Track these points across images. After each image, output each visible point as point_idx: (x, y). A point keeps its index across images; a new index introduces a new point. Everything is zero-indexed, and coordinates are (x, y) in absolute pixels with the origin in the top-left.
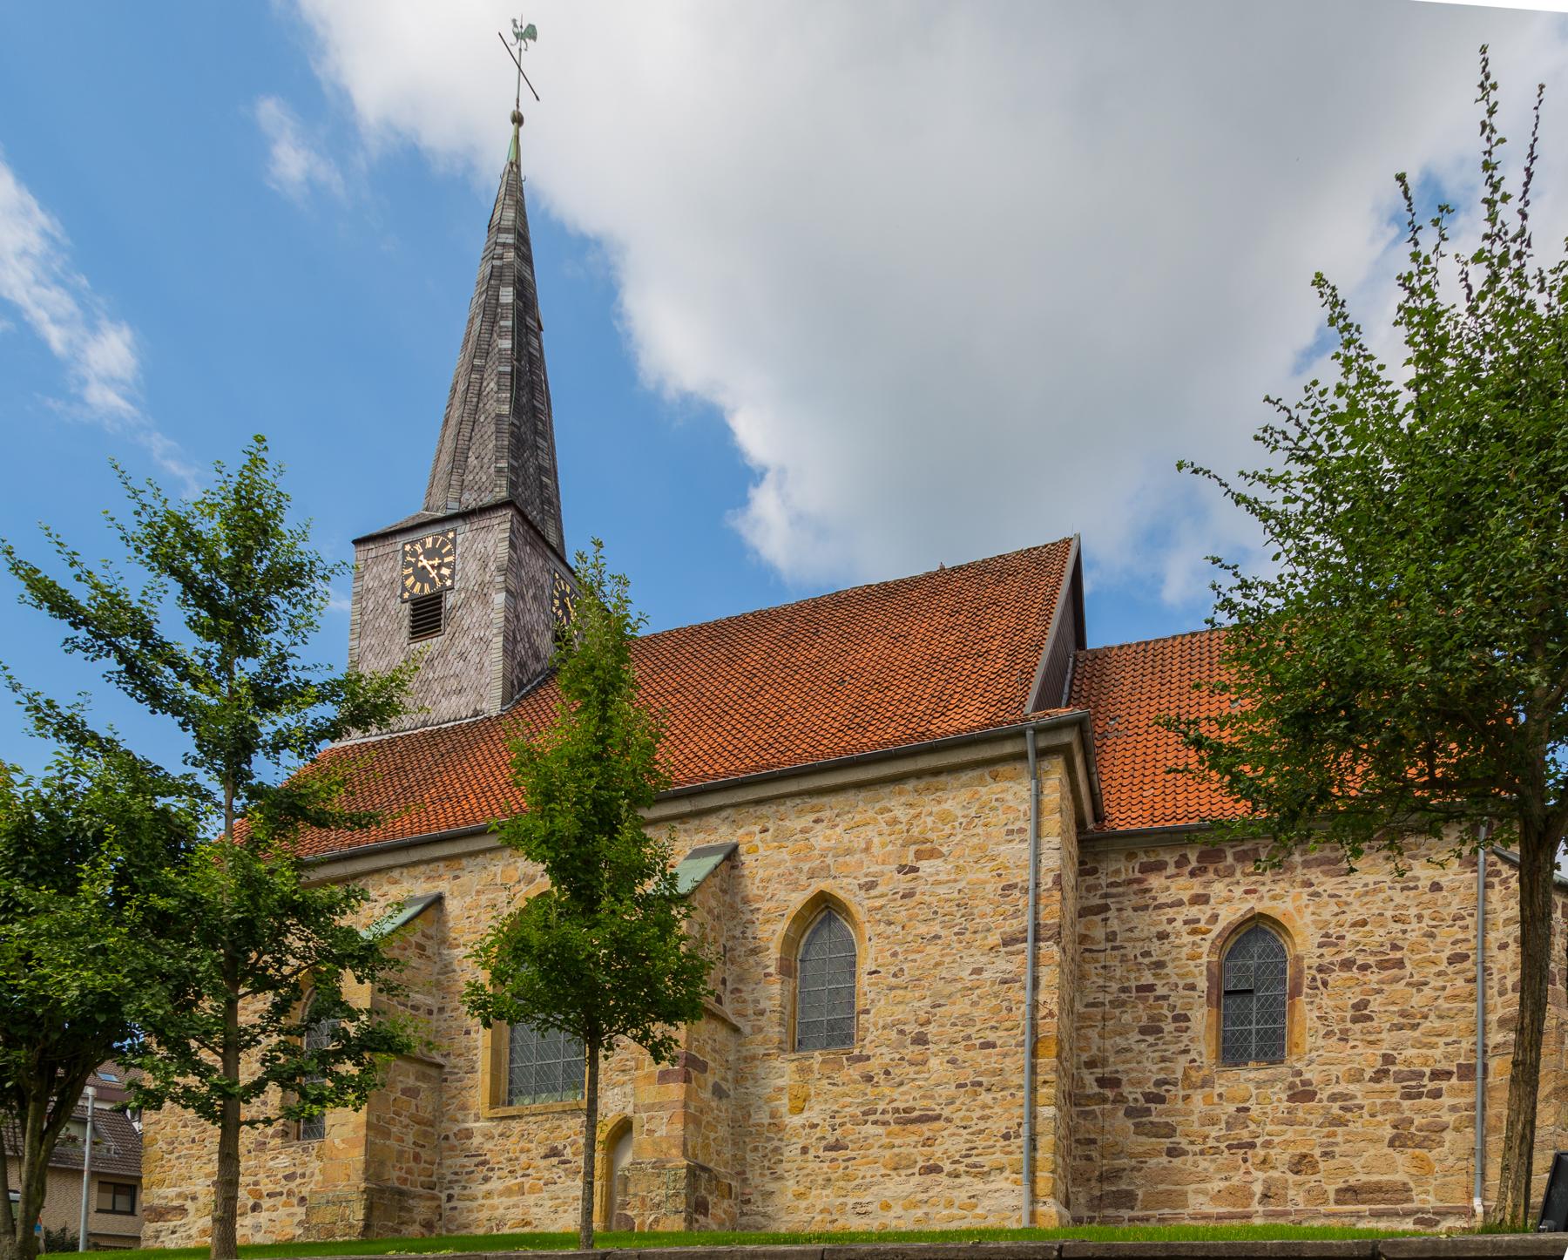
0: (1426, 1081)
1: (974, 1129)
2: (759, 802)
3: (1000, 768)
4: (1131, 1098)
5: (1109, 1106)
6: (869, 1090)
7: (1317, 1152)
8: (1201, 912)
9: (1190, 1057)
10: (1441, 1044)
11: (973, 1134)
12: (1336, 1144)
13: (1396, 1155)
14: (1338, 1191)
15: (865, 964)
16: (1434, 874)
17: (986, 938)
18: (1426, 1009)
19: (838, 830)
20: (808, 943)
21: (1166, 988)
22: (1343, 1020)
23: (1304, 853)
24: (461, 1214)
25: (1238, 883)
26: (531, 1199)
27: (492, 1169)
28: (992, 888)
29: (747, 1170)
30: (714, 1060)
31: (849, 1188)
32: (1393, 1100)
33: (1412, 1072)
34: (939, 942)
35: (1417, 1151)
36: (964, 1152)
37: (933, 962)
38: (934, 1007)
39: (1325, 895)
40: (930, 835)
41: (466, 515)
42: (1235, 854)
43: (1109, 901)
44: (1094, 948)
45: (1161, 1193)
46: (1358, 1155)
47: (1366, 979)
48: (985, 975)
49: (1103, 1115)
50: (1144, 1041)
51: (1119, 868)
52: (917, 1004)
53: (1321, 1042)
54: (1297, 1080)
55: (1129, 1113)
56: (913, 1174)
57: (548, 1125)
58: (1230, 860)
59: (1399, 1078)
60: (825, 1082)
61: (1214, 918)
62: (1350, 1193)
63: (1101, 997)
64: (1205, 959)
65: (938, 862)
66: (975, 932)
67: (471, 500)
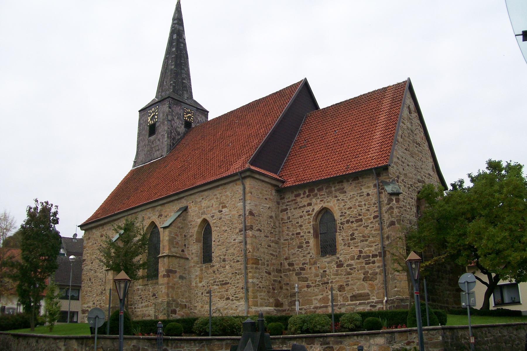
0: (371, 258)
2: (191, 195)
5: (291, 272)
10: (374, 246)
12: (349, 281)
13: (365, 284)
14: (351, 297)
18: (369, 234)
19: (207, 201)
21: (303, 233)
22: (348, 240)
25: (318, 198)
32: (363, 265)
35: (370, 282)
37: (225, 238)
38: (226, 251)
39: (341, 200)
42: (317, 189)
43: (288, 207)
44: (285, 222)
46: (355, 284)
47: (353, 226)
48: (236, 241)
50: (299, 250)
51: (290, 197)
53: (343, 248)
54: (338, 260)
58: (316, 191)
59: (364, 258)
60: (206, 273)
61: (313, 210)
62: (354, 297)
63: (287, 237)
64: (312, 223)
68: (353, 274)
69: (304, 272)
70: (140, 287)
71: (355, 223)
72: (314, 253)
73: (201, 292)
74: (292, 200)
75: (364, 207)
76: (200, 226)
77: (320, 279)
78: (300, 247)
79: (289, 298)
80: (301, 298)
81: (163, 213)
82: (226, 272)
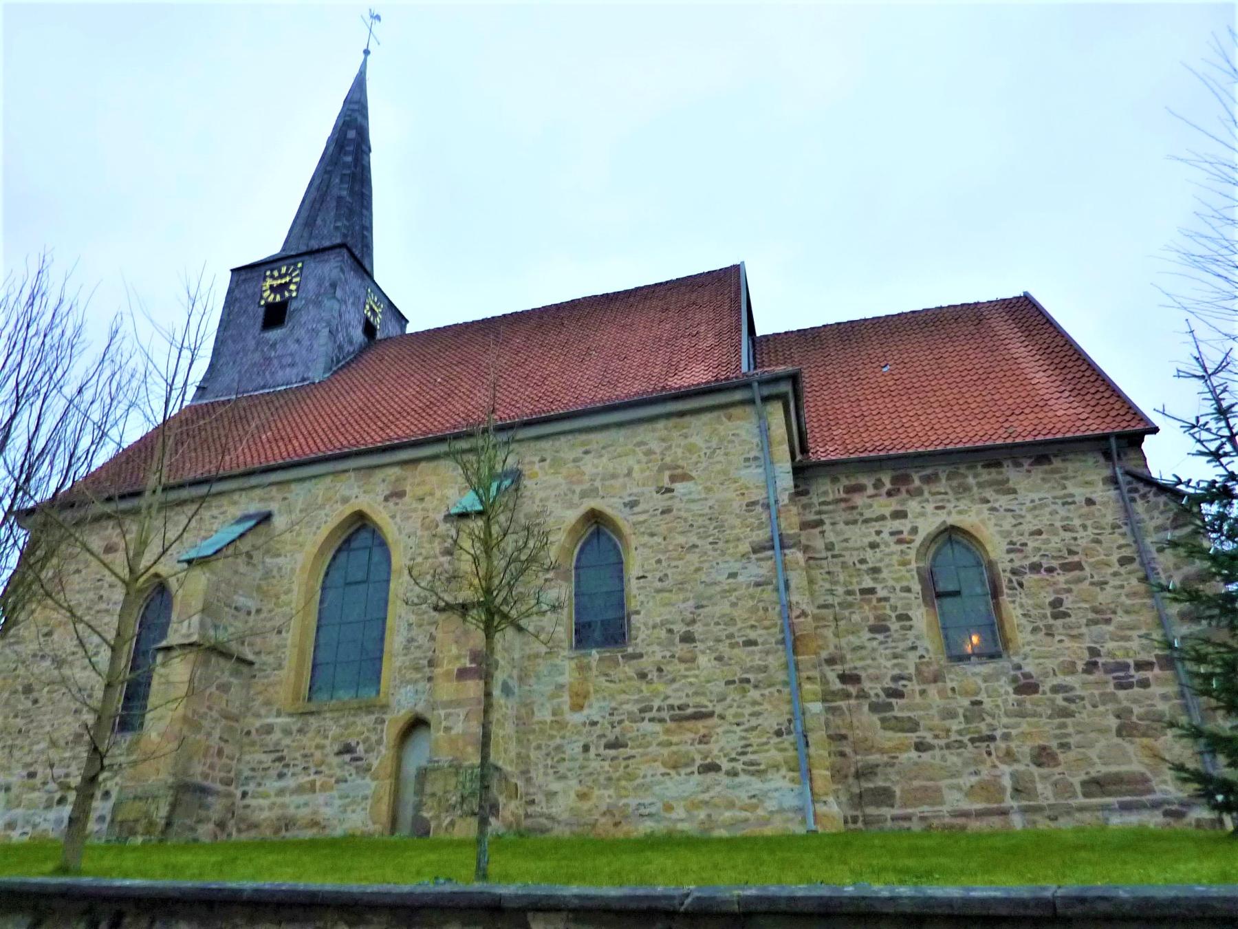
1: (747, 726)
3: (732, 411)
4: (872, 693)
5: (853, 702)
6: (644, 687)
7: (1054, 744)
8: (904, 525)
9: (918, 653)
11: (746, 730)
13: (1126, 744)
14: (1083, 784)
15: (633, 569)
16: (1087, 492)
17: (737, 546)
19: (604, 459)
20: (582, 550)
23: (975, 476)
24: (253, 811)
25: (927, 501)
26: (320, 798)
27: (287, 766)
28: (738, 504)
29: (532, 769)
30: (504, 658)
31: (630, 788)
33: (1117, 663)
34: (697, 550)
35: (1145, 741)
36: (740, 750)
37: (693, 568)
38: (698, 607)
39: (1002, 510)
40: (680, 463)
41: (311, 253)
43: (823, 517)
45: (916, 789)
46: (1091, 745)
47: (1054, 580)
48: (740, 579)
49: (850, 710)
50: (874, 639)
51: (825, 490)
52: (682, 606)
53: (1030, 638)
54: (1019, 673)
55: (874, 708)
56: (693, 773)
57: (343, 722)
58: (917, 483)
59: (1108, 669)
60: (603, 679)
61: (914, 530)
63: (830, 599)
64: (914, 565)
65: (690, 484)
66: (727, 542)
67: (315, 245)
68: (1077, 715)
69: (901, 701)
70: (279, 720)
71: (1059, 571)
72: (930, 648)
73: (582, 744)
74: (838, 501)
75: (1081, 533)
76: (573, 530)
77: (962, 726)
78: (879, 628)
79: (851, 780)
80: (898, 782)
81: (408, 489)
82: (696, 676)
